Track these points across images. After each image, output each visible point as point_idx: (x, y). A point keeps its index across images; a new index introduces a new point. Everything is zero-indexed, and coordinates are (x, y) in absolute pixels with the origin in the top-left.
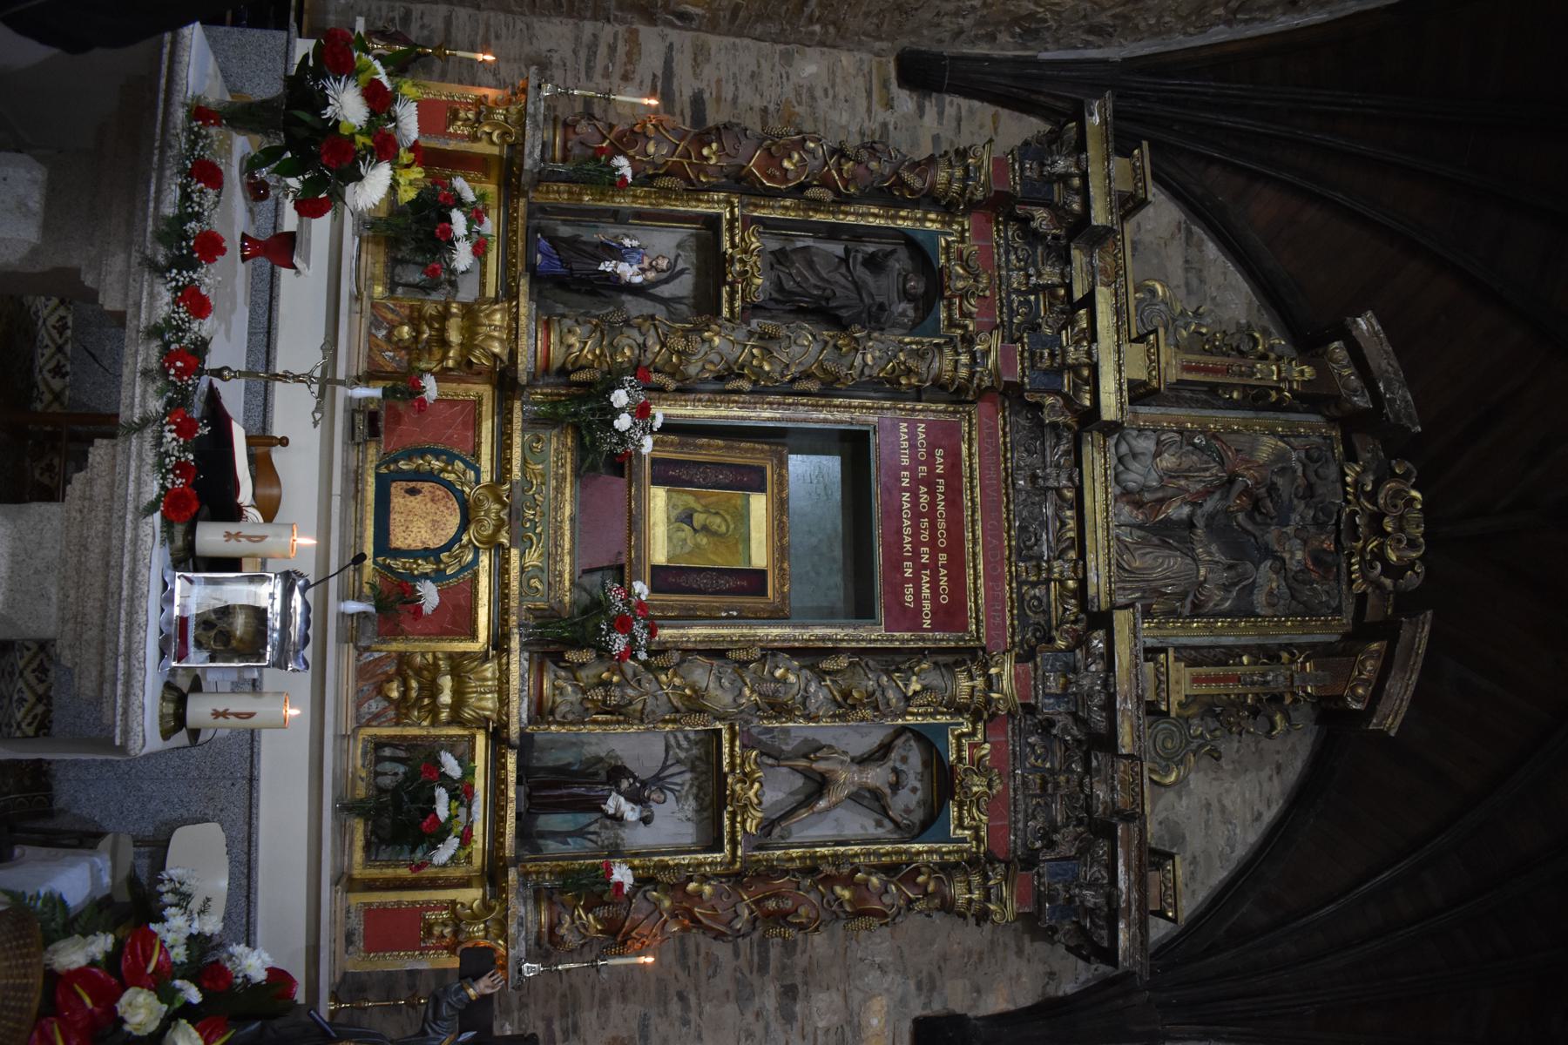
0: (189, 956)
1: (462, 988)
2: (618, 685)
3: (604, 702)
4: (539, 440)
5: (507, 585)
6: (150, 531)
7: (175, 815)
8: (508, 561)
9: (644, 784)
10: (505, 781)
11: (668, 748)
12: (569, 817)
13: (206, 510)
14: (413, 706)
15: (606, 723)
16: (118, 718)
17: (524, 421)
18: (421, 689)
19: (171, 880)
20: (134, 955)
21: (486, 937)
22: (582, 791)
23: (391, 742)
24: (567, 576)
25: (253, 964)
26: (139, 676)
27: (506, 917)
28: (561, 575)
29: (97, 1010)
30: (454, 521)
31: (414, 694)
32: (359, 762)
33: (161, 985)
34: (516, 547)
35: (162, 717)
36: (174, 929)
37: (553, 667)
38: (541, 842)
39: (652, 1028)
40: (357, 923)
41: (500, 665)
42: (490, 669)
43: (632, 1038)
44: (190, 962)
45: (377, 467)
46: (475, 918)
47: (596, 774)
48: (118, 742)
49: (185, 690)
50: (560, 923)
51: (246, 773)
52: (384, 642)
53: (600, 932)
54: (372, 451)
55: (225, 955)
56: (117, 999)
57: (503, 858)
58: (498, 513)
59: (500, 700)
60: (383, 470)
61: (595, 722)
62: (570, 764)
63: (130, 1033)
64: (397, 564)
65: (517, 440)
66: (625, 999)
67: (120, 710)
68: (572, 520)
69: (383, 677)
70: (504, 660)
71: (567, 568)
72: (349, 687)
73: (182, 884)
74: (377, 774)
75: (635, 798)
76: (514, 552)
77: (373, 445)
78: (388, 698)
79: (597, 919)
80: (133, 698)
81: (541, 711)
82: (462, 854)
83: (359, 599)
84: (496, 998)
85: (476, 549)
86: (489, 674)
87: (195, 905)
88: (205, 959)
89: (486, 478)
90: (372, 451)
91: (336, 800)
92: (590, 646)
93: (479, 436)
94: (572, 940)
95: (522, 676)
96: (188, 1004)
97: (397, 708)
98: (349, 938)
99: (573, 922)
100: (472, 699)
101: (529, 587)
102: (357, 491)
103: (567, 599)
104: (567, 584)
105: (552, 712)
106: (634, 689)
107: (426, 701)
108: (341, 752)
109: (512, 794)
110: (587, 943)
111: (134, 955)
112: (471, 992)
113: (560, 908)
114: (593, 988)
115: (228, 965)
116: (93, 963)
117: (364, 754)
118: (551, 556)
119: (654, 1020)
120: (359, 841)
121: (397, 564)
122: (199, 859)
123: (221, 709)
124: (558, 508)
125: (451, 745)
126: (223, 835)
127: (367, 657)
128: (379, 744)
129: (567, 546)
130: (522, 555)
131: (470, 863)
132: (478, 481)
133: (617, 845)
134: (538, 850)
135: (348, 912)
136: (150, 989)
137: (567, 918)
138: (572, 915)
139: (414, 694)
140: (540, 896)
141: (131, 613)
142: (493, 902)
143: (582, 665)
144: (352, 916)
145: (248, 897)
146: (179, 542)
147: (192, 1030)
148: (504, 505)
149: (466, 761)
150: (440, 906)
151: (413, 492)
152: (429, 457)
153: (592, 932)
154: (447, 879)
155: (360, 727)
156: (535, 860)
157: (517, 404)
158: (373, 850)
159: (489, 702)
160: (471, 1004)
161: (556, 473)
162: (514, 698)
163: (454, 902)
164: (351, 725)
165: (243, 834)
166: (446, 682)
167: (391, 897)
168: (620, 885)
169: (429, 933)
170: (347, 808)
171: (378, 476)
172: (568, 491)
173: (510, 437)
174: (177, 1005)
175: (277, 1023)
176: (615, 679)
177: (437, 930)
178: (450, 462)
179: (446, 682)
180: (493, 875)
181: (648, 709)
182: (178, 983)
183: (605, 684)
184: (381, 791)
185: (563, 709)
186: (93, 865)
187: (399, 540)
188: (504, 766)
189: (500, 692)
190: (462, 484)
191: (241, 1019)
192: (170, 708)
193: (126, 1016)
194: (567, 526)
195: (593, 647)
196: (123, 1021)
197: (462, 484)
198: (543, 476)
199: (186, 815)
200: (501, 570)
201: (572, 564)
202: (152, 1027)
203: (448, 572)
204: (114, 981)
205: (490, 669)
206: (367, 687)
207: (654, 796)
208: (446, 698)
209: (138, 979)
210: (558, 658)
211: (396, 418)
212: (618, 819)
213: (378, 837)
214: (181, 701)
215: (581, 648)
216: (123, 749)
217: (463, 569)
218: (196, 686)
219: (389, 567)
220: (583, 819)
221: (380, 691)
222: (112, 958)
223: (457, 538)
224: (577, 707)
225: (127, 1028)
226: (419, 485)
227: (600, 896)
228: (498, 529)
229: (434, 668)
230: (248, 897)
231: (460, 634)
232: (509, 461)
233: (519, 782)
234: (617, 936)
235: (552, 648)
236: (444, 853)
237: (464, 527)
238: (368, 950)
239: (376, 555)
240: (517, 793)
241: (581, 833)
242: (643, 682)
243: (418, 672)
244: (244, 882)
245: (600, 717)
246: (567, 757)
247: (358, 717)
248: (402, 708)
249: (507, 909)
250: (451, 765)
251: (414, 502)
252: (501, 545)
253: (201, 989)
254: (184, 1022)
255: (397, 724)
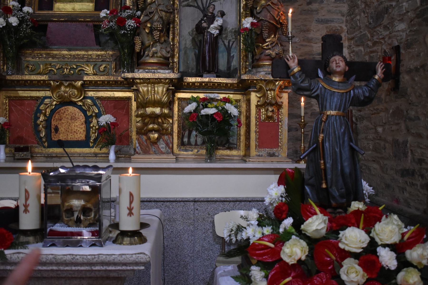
0: (269, 225)
1: (294, 75)
2: (152, 24)
3: (161, 31)
4: (28, 67)
5: (103, 82)
6: (16, 256)
7: (211, 235)
8: (91, 82)
9: (205, 16)
10: (201, 83)
11: (189, 5)
12: (220, 55)
13: (13, 226)
14: (162, 126)
15: (174, 34)
16: (129, 268)
17: (18, 74)
18: (154, 123)
19: (230, 236)
20: (264, 254)
21: (274, 90)
22: (207, 48)
23: (181, 137)
24: (99, 53)
25: (275, 192)
26: (103, 258)
27: (265, 80)
28: (98, 56)
29: (292, 275)
30: (71, 109)
31: (156, 126)
32: (190, 153)
33: (280, 240)
34: (83, 77)
35: (131, 244)
36: (253, 233)
37: (143, 58)
38: (232, 68)
39: (323, 18)
40: (264, 152)
41: (140, 83)
42: (143, 89)
43: (327, 28)
44: (273, 225)
45: (44, 147)
46: (264, 96)
47: (200, 41)
48: (143, 268)
49: (118, 232)
50: (269, 55)
51: (192, 204)
52: (132, 142)
53: (275, 36)
54: (37, 150)
55: (270, 207)
56: (287, 264)
57: (238, 84)
58: (66, 87)
59: (158, 83)
60: (46, 144)
61: (173, 39)
62: (195, 54)
63: (307, 256)
64: (93, 136)
65: (27, 77)
66: (308, 31)
67: (124, 268)
68: (70, 50)
69: (148, 141)
70: (138, 81)
71: (95, 52)
72: (153, 157)
73: (232, 230)
74: (196, 144)
75: (211, 19)
76: (85, 78)
77: (33, 149)
78: (158, 139)
79: (269, 37)
80: (116, 261)
81: (165, 64)
82: (234, 103)
83: (108, 154)
84: (301, 58)
85: (85, 98)
86: (145, 89)
87: (243, 223)
88: (271, 217)
89: (48, 93)
90: (37, 150)
91: (206, 162)
92: (133, 40)
93: (27, 97)
94: (278, 49)
95: (147, 72)
96: (293, 225)
97: (163, 135)
98: (272, 155)
99: (270, 49)
100: (157, 97)
101: (104, 71)
102: (57, 156)
103: (111, 53)
104: (103, 53)
105: (167, 59)
106: (154, 16)
107: (160, 120)
108: (185, 160)
109: (207, 80)
110: (280, 42)
111: (264, 254)
112: (296, 70)
113: (263, 56)
114: (302, 45)
115: (275, 205)
116: (266, 277)
117: (186, 150)
118: (88, 61)
119: (320, 16)
120: (228, 152)
121: (93, 136)
122: (224, 224)
123: (128, 211)
124: (64, 56)
125: (181, 108)
126: (220, 213)
127: (138, 150)
128: (182, 144)
129: (83, 53)
130: (87, 74)
131: (239, 100)
132: (50, 98)
133: (235, 32)
134: (236, 70)
135: (259, 156)
136: (283, 245)
137: (267, 51)
138: (267, 49)
139: (156, 126)
140: (255, 65)
141: (66, 264)
142: (258, 87)
143: (143, 43)
144: (261, 154)
145: (250, 201)
146: (31, 239)
147: (307, 222)
148: (61, 84)
149: (188, 101)
150: (258, 113)
151: (57, 130)
152: (38, 122)
153: (275, 40)
154: (246, 111)
155: (173, 152)
156: (240, 70)
157: (8, 78)
158: (231, 146)
159: (160, 89)
160: (303, 71)
161: (45, 58)
162: (157, 76)
163: (257, 106)
164: (171, 156)
165: (221, 204)
166: (149, 110)
167: (253, 135)
168: (252, 24)
169: (270, 118)
170: (210, 156)
171: (49, 147)
172: (55, 52)
173: (26, 81)
174: (293, 230)
175: (306, 177)
176: (149, 25)
177: (270, 114)
178: (40, 111)
179: (149, 110)
180: (244, 88)
181: (165, 9)
182: (281, 230)
183: (152, 30)
184: (204, 143)
185: (164, 53)
186: (222, 276)
187: (81, 136)
188: (193, 83)
189: (154, 83)
190: (52, 105)
191: (303, 197)
192: (127, 240)
193: (297, 258)
194: (73, 53)
195: (133, 37)
196: (299, 261)
197: (52, 105)
198: (46, 64)
199: (211, 230)
200: (96, 85)
201: (93, 50)
202: (304, 243)
203: (97, 111)
204: (277, 266)
205: (143, 89)
206: (153, 149)
207: (211, 10)
208: (157, 110)
209: (276, 252)
210: (140, 56)
211: (20, 139)
212: (221, 29)
213: (226, 144)
214: (124, 234)
215: (134, 44)
216: (147, 264)
217: (95, 104)
218: (116, 226)
219: (95, 140)
220: (221, 48)
221: (155, 143)
222: (264, 266)
223: (80, 107)
224: (164, 46)
225: (303, 258)
226: (53, 127)
227: (258, 35)
228: (74, 87)
229: (143, 116)
230: (250, 201)
231: (128, 105)
232: (39, 81)
233: (201, 76)
234: (277, 27)
235: (135, 60)
236: (233, 110)
237: (74, 104)
238: (278, 146)
239: (89, 147)
240: (206, 77)
241: (229, 49)
242: (151, 11)
243: (146, 124)
244: (243, 203)
245: (171, 37)
246: (192, 55)
247: (168, 153)
248: (164, 132)
249: (261, 80)
250: (191, 108)
251: (62, 129)
252: (82, 85)
253: (286, 218)
254: (302, 227)
255: (172, 135)
